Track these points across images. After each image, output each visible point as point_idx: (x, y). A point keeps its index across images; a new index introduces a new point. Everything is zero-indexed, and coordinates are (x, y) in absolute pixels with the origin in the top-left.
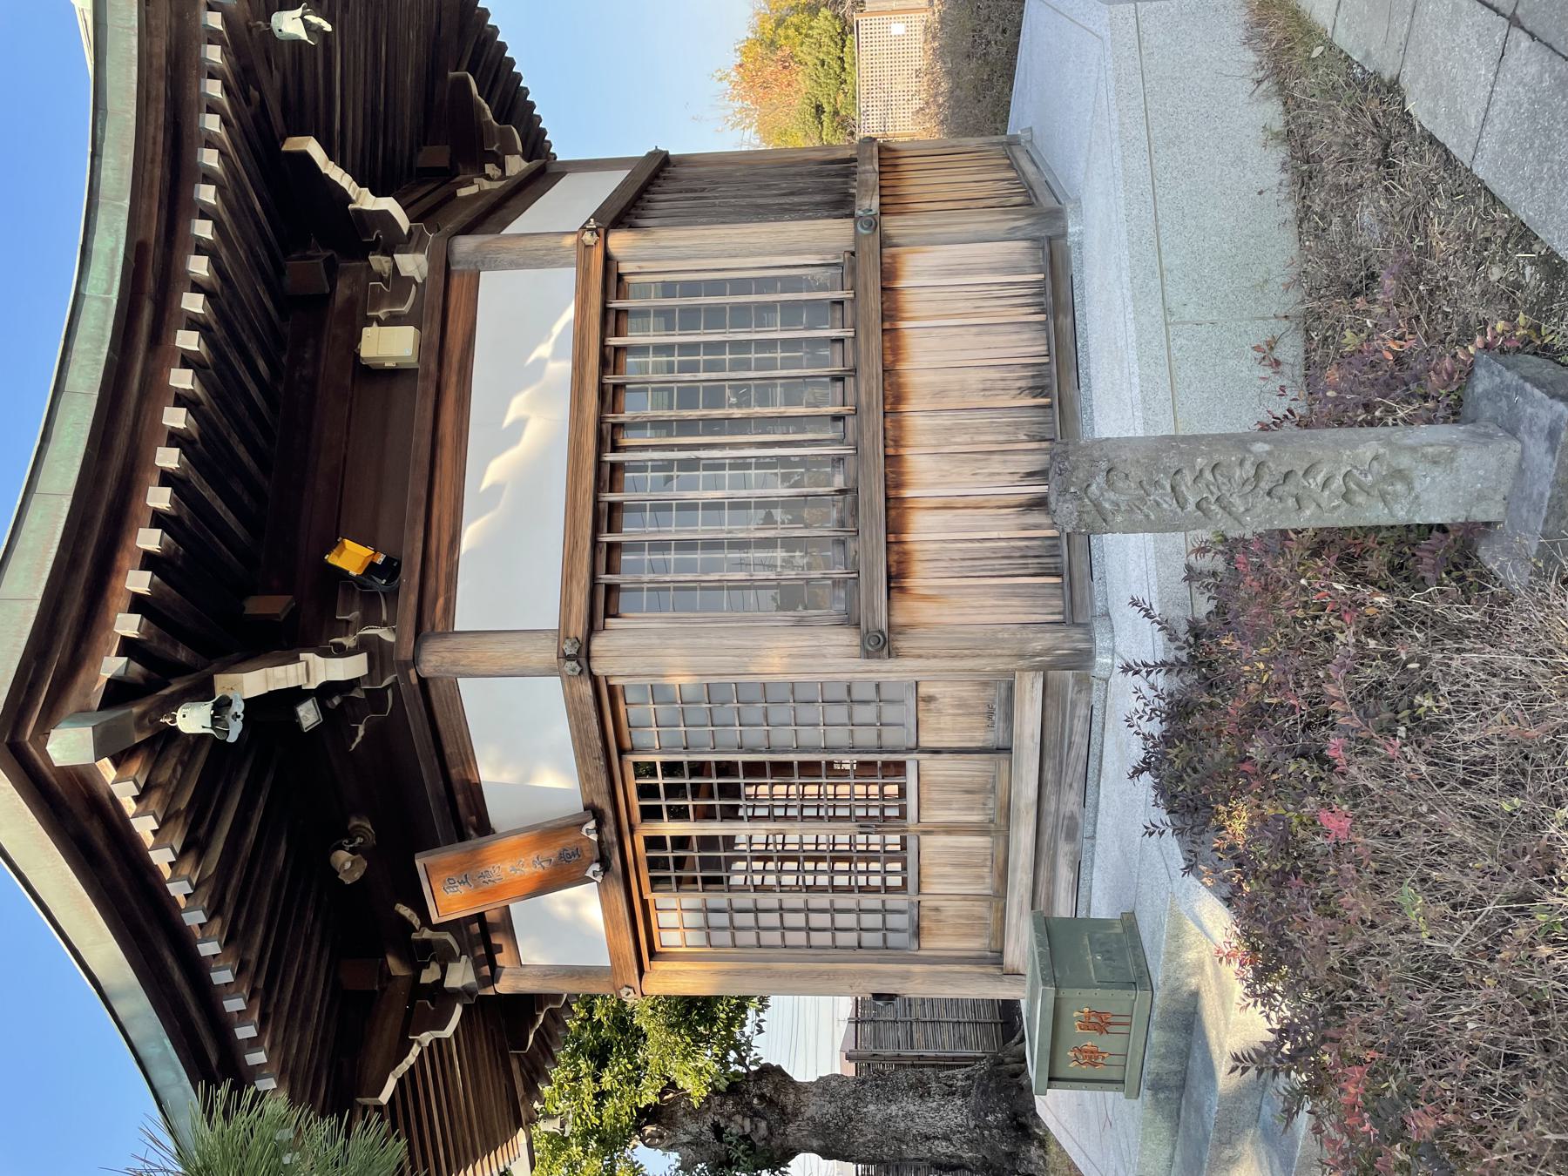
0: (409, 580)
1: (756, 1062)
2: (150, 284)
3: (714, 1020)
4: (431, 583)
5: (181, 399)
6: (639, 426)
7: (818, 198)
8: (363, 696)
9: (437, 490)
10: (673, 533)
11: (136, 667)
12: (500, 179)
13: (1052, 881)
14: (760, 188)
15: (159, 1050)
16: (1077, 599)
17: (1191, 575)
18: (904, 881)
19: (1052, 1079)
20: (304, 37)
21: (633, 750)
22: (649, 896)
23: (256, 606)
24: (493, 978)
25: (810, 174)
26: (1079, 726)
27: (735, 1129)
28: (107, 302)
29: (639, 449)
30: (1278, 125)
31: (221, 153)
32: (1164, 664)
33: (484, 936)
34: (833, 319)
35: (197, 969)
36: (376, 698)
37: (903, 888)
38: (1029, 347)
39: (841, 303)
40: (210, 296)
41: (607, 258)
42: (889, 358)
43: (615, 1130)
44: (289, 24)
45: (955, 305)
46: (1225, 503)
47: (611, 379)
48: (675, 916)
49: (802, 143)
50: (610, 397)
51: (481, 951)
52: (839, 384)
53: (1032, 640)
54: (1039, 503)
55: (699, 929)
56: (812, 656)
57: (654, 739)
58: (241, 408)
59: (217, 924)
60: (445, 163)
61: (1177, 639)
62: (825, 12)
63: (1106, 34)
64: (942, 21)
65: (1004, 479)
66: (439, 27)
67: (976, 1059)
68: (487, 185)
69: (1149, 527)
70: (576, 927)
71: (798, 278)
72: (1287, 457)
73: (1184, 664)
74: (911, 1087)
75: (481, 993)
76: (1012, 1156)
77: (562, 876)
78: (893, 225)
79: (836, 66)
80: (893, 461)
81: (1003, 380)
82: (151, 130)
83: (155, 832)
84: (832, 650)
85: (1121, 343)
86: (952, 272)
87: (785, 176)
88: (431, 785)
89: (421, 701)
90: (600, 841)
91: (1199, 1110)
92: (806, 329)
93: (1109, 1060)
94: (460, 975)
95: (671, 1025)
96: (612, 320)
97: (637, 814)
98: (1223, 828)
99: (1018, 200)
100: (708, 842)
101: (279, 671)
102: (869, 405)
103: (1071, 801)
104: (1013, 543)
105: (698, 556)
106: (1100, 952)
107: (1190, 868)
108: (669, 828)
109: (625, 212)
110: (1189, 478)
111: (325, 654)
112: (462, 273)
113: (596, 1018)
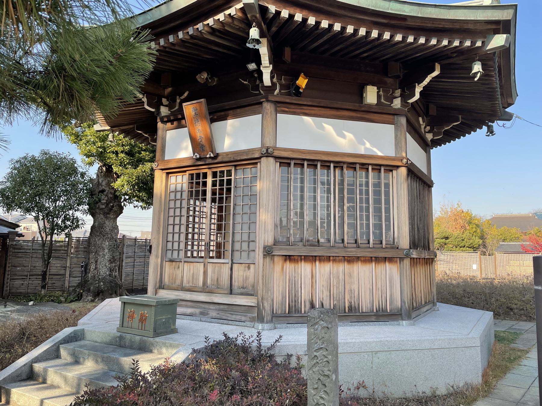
0: (295, 100)
1: (124, 205)
2: (393, 22)
3: (139, 191)
4: (293, 107)
5: (356, 31)
6: (342, 175)
7: (416, 237)
8: (257, 83)
9: (323, 109)
10: (307, 185)
11: (271, 16)
12: (425, 131)
13: (187, 306)
14: (420, 218)
15: (149, 18)
16: (281, 319)
17: (289, 356)
18: (189, 257)
19: (124, 303)
20: (473, 72)
21: (236, 170)
22: (187, 173)
23: (288, 51)
24: (163, 122)
25: (424, 234)
26: (238, 317)
27: (103, 197)
28: (388, 9)
29: (334, 175)
30: (438, 393)
31: (435, 45)
32: (260, 345)
33: (177, 119)
34: (376, 241)
35: (174, 31)
36: (256, 88)
37: (192, 256)
38: (365, 305)
39: (381, 243)
40: (389, 41)
41: (398, 167)
42: (362, 259)
43: (105, 157)
44: (477, 68)
45: (377, 282)
46: (316, 365)
47: (358, 166)
48: (180, 181)
49: (435, 232)
50: (352, 166)
51: (172, 118)
52: (354, 242)
53: (268, 303)
54: (312, 306)
55: (176, 189)
56: (265, 230)
57: (239, 177)
58: (352, 48)
59: (188, 37)
60: (430, 114)
61: (268, 350)
62: (481, 241)
63: (470, 336)
64: (477, 282)
65: (321, 296)
66: (477, 113)
67: (121, 280)
68: (423, 127)
69: (309, 340)
70: (178, 148)
71: (390, 229)
72: (331, 385)
73: (260, 352)
74: (113, 257)
75: (158, 118)
76: (89, 290)
77: (196, 145)
78: (407, 262)
79: (462, 245)
80: (328, 259)
82: (444, 23)
83: (219, 19)
84: (267, 236)
85: (366, 336)
87: (424, 226)
88: (227, 104)
89: (255, 102)
90: (207, 158)
91: (113, 351)
92: (373, 232)
93: (130, 322)
94: (164, 111)
95: (139, 177)
96: (377, 168)
97: (215, 170)
98: (207, 363)
99: (415, 305)
100: (204, 193)
101: (267, 58)
102: (347, 251)
103: (213, 314)
104: (300, 298)
105: (299, 193)
106: (164, 321)
107: (194, 351)
108: (209, 180)
109: (413, 173)
110: (325, 353)
111: (272, 73)
112: (394, 119)
113: (142, 152)
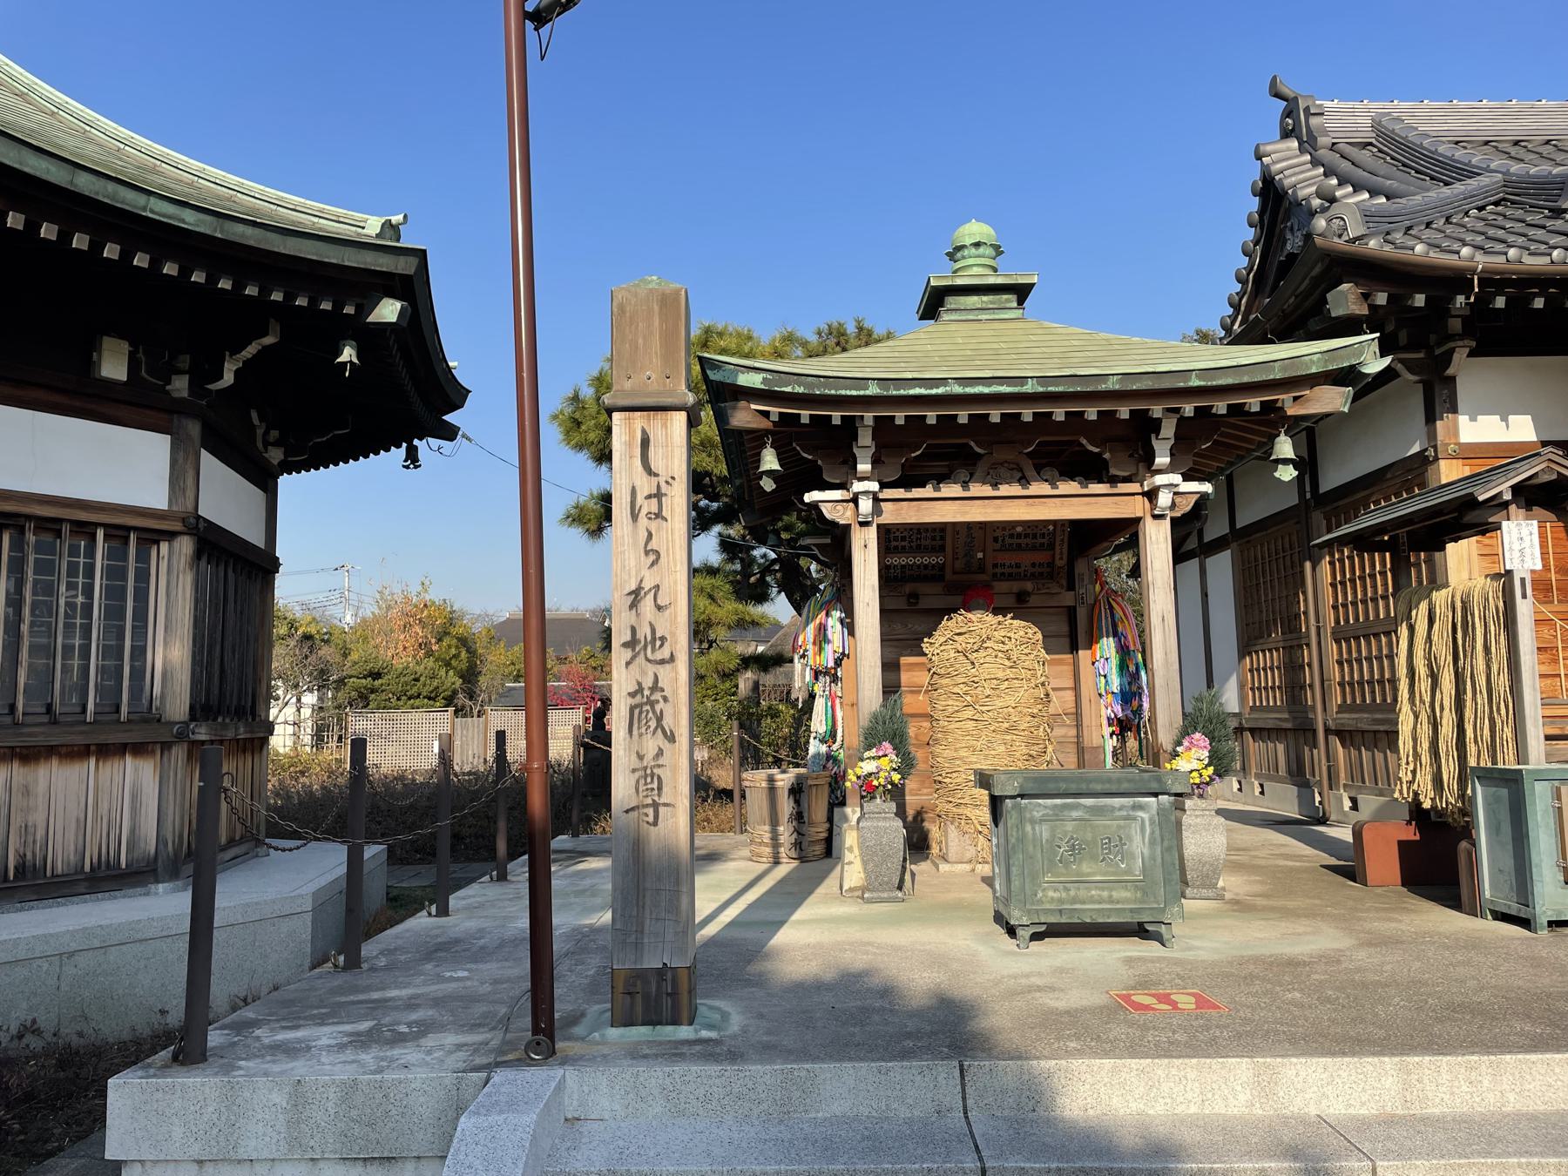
28: (144, 209)
38: (61, 856)
42: (64, 750)
47: (66, 528)
68: (260, 432)
79: (414, 691)
81: (34, 842)
86: (135, 797)
102: (22, 734)
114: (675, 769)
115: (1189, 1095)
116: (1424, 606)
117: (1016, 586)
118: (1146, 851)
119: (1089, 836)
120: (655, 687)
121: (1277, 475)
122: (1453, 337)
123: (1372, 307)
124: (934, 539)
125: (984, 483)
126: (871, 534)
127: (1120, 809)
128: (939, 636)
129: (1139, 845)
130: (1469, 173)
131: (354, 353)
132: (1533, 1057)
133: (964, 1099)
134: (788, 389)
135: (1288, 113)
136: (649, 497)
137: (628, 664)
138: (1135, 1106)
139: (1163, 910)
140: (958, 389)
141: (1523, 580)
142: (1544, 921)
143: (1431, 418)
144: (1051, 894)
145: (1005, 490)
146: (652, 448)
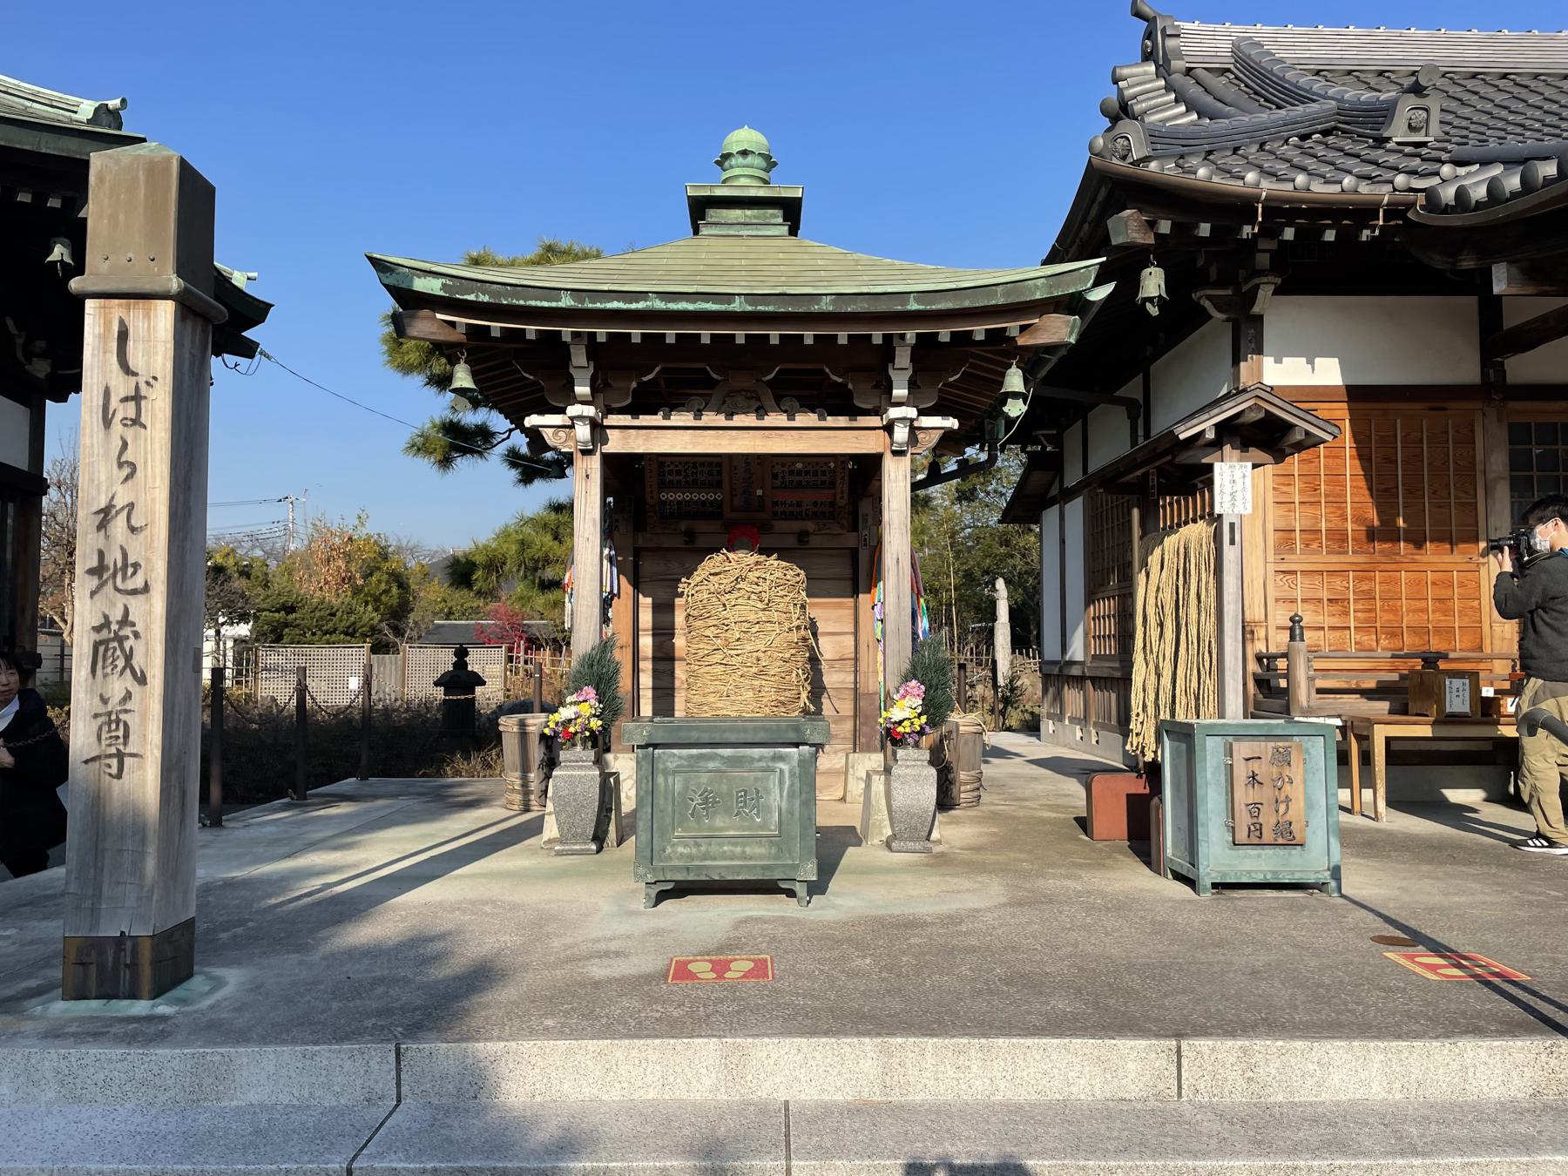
68: (19, 341)
114: (144, 716)
115: (649, 1079)
116: (1157, 552)
117: (796, 526)
118: (784, 805)
119: (724, 788)
120: (125, 621)
121: (1005, 409)
122: (1261, 273)
123: (1158, 236)
124: (710, 473)
125: (719, 412)
126: (595, 463)
127: (760, 760)
128: (700, 573)
129: (776, 798)
130: (1304, 98)
131: (66, 252)
132: (1029, 1041)
133: (398, 1085)
134: (472, 297)
135: (1149, 35)
136: (125, 399)
137: (93, 594)
138: (587, 1092)
139: (795, 867)
140: (659, 305)
141: (1232, 525)
142: (1208, 882)
143: (1236, 361)
144: (680, 849)
145: (739, 420)
146: (130, 343)
